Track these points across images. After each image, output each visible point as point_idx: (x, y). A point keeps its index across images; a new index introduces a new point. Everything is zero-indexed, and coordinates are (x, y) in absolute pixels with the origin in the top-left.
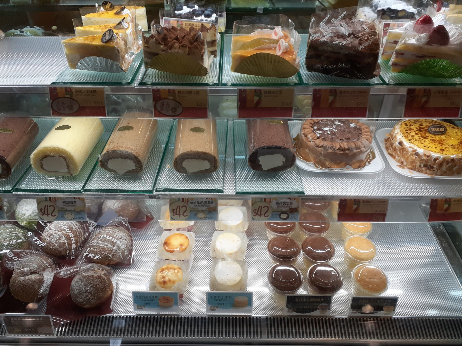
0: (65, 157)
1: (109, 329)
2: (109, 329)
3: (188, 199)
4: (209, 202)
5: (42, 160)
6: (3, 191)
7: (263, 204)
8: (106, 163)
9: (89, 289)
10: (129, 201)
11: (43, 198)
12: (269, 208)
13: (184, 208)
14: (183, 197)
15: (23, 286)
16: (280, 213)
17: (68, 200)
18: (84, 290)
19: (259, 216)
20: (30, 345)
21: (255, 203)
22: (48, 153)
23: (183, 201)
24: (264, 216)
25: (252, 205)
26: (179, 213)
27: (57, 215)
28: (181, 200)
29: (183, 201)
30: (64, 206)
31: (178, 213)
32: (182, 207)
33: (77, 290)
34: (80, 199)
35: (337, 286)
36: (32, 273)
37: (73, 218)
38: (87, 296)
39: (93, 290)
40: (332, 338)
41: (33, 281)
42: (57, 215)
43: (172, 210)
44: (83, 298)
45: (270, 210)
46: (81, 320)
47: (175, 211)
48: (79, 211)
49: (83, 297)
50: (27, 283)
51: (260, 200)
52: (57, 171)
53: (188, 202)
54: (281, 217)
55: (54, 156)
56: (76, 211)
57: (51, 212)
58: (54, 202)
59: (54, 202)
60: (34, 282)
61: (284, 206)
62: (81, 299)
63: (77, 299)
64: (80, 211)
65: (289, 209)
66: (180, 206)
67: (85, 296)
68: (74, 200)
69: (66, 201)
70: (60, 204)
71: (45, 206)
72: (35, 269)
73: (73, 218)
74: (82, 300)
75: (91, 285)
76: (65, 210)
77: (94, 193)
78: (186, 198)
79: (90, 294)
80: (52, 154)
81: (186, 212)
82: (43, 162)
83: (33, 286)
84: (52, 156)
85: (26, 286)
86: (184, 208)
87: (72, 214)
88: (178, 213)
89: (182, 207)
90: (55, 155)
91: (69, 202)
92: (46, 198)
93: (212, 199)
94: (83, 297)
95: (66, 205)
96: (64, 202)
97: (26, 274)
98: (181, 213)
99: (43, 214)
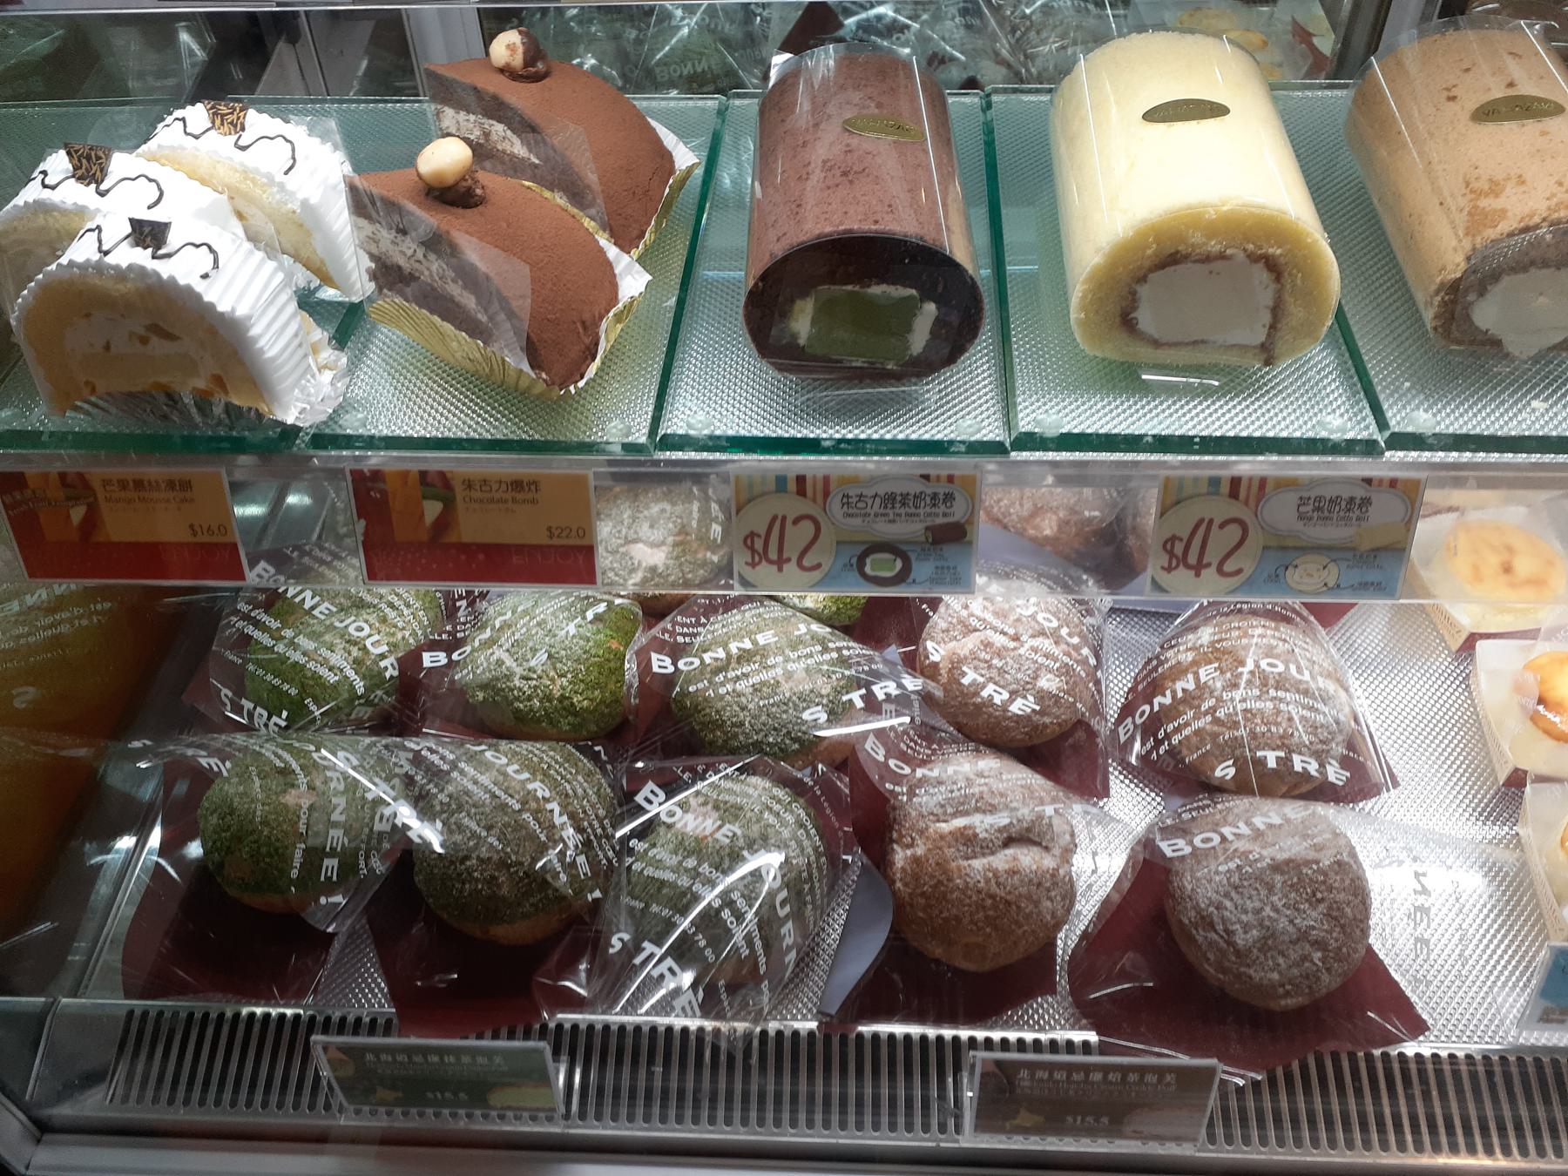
0: (1282, 260)
1: (295, 1074)
2: (295, 1074)
3: (826, 479)
4: (935, 496)
5: (1143, 279)
6: (963, 448)
7: (1221, 509)
8: (1471, 297)
9: (1313, 928)
10: (1087, 492)
11: (1196, 480)
12: (1251, 532)
13: (1234, 532)
14: (827, 472)
15: (995, 907)
16: (863, 548)
17: (1327, 493)
18: (1290, 929)
19: (775, 568)
20: (389, 1140)
21: (1178, 502)
22: (1197, 238)
23: (801, 491)
24: (1220, 571)
25: (1162, 513)
26: (780, 550)
27: (825, 568)
28: (792, 486)
29: (801, 491)
30: (1301, 523)
31: (773, 555)
32: (796, 522)
33: (1246, 928)
34: (1398, 485)
35: (1333, 914)
36: (1009, 842)
37: (1331, 584)
38: (1305, 958)
39: (1330, 932)
40: (1489, 1151)
41: (1035, 881)
42: (825, 568)
43: (1164, 546)
44: (1284, 966)
45: (1255, 539)
46: (1304, 1068)
47: (759, 544)
48: (1373, 550)
49: (1281, 960)
50: (1010, 893)
51: (773, 487)
52: (1203, 342)
53: (826, 494)
54: (868, 570)
55: (1222, 256)
56: (1354, 549)
57: (1219, 558)
58: (1252, 503)
59: (1252, 503)
60: (1039, 885)
61: (918, 515)
62: (1272, 970)
63: (1251, 972)
64: (1378, 549)
65: (927, 529)
66: (784, 518)
67: (1293, 956)
68: (1359, 493)
69: (1319, 499)
70: (1280, 510)
71: (775, 518)
72: (1025, 825)
73: (1331, 584)
74: (1275, 976)
75: (1322, 908)
76: (1298, 544)
77: (1440, 456)
78: (820, 475)
79: (1318, 950)
80: (1214, 246)
81: (809, 554)
82: (1144, 291)
83: (1037, 903)
84: (1207, 259)
85: (1008, 903)
86: (807, 528)
87: (1332, 566)
88: (773, 555)
89: (796, 522)
90: (1229, 252)
91: (1334, 501)
92: (1215, 482)
93: (950, 479)
94: (1281, 960)
95: (1311, 519)
96: (1303, 501)
97: (987, 848)
98: (791, 551)
99: (757, 559)
